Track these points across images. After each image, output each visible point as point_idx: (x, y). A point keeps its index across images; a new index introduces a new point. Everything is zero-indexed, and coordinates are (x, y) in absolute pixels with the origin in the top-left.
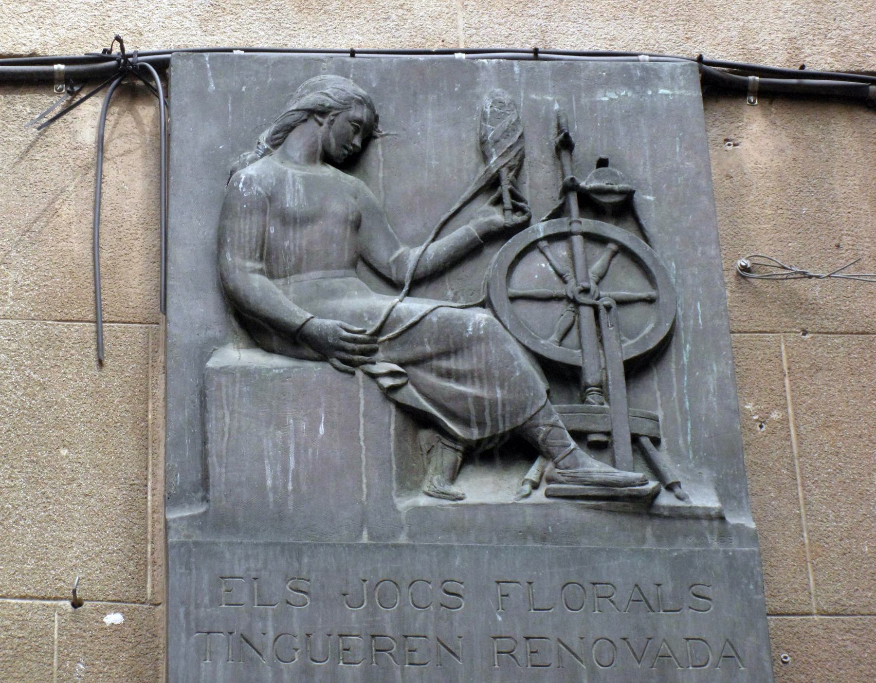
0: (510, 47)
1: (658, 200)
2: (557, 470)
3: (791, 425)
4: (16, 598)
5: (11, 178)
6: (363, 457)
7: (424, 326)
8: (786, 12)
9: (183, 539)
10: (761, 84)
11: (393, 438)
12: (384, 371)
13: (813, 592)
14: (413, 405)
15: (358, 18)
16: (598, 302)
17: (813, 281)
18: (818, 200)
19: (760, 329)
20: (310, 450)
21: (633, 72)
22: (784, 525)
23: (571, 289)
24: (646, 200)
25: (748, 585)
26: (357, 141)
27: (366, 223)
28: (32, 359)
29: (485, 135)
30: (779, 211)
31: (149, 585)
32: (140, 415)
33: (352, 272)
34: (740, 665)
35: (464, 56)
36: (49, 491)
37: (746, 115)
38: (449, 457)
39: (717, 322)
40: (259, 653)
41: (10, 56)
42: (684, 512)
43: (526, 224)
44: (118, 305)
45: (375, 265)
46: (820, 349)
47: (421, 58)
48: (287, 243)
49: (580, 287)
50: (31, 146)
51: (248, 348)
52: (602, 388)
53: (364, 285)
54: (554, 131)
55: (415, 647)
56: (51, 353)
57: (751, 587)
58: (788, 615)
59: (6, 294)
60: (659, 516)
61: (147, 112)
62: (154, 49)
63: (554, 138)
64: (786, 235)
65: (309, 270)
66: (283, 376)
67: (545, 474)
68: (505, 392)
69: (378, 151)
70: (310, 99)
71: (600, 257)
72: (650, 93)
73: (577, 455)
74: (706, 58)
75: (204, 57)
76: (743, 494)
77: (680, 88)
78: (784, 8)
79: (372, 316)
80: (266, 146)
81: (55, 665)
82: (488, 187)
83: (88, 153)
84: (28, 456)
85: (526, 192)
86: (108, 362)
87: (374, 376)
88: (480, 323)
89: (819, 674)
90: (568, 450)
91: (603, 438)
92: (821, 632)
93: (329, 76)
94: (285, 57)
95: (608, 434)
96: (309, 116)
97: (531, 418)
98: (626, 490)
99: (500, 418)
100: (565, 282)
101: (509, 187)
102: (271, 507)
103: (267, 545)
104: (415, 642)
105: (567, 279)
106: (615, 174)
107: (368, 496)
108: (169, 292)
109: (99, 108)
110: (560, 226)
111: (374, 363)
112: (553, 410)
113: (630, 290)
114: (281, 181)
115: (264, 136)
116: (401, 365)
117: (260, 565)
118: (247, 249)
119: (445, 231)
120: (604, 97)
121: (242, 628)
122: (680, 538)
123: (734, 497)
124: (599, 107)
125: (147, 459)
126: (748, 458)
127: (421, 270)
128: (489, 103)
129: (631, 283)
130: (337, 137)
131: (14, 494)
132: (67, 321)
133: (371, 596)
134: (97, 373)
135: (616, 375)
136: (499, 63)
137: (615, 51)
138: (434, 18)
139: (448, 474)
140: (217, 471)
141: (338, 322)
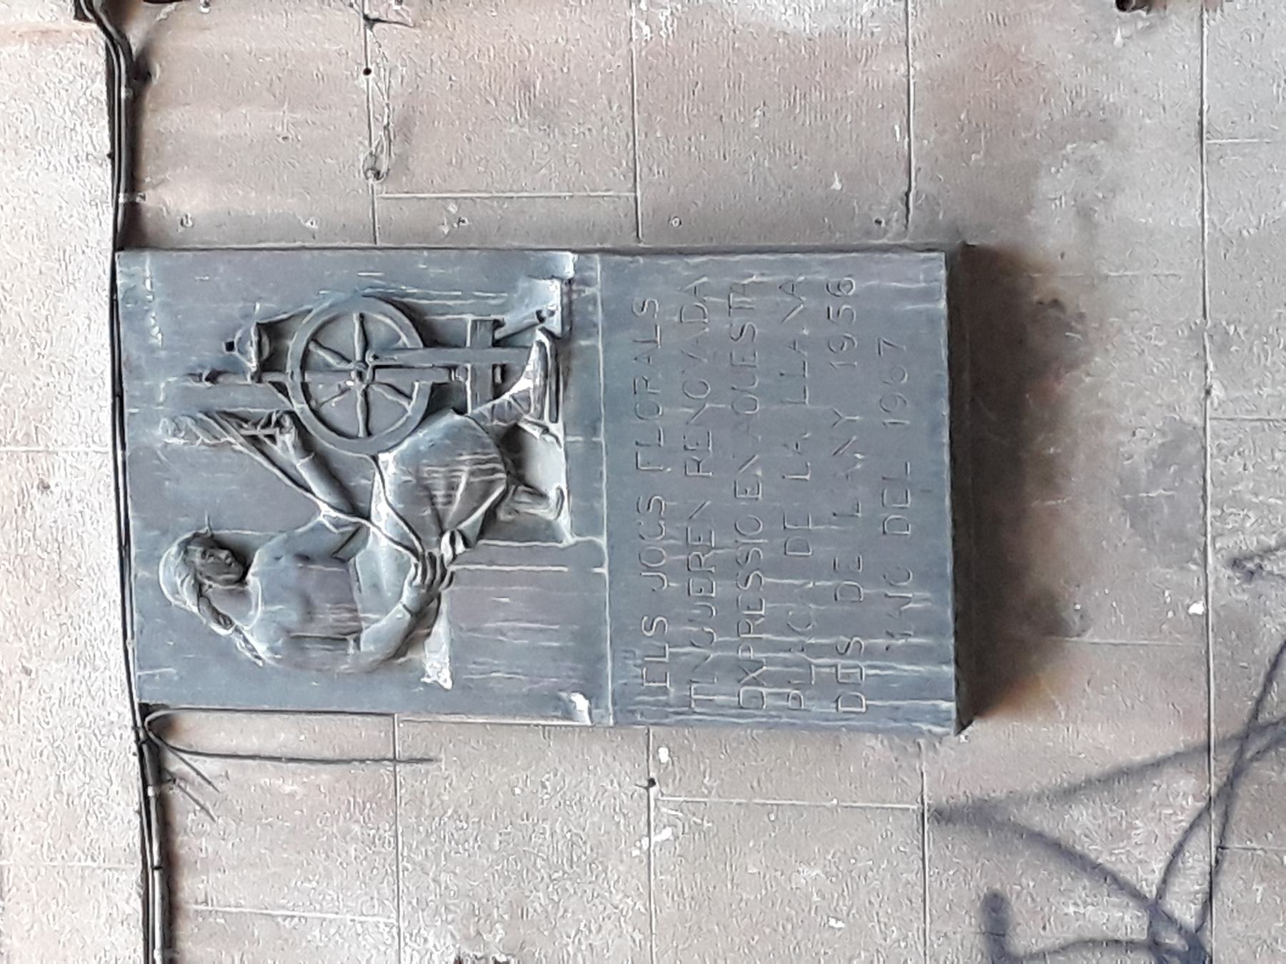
1: (259, 299)
16: (370, 365)
26: (223, 554)
43: (292, 414)
52: (451, 368)
80: (230, 631)
82: (333, 521)
88: (401, 470)
91: (498, 371)
95: (494, 367)
115: (221, 631)
116: (442, 533)
119: (302, 482)
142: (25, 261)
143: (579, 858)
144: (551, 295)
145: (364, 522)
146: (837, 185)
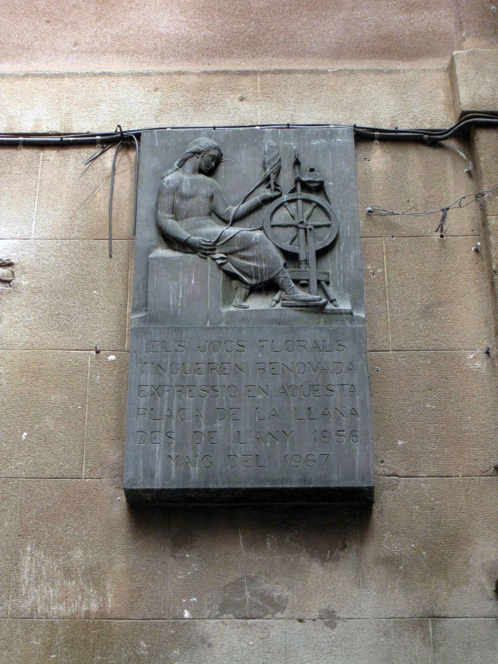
0: (279, 124)
2: (286, 296)
3: (386, 274)
4: (74, 350)
5: (78, 182)
6: (209, 292)
7: (235, 239)
8: (391, 106)
9: (136, 326)
10: (380, 135)
11: (221, 284)
12: (218, 257)
13: (390, 342)
14: (230, 271)
15: (218, 113)
17: (397, 216)
18: (401, 182)
19: (374, 236)
20: (188, 290)
21: (327, 132)
22: (380, 315)
23: (296, 222)
24: (329, 185)
25: (360, 340)
26: (213, 164)
27: (215, 197)
28: (83, 255)
29: (265, 160)
30: (385, 187)
31: (126, 344)
32: (125, 276)
33: (209, 217)
34: (355, 372)
35: (259, 127)
36: (88, 308)
37: (373, 148)
38: (244, 291)
39: (356, 234)
40: (164, 371)
41: (79, 134)
42: (336, 311)
43: (280, 195)
44: (118, 232)
45: (218, 214)
46: (399, 243)
47: (241, 129)
48: (182, 207)
49: (299, 221)
50: (86, 170)
51: (166, 249)
52: (306, 261)
53: (213, 222)
54: (293, 157)
55: (226, 367)
56: (91, 253)
57: (361, 341)
58: (380, 351)
59: (74, 229)
60: (326, 313)
61: (132, 154)
62: (136, 129)
63: (293, 160)
64: (388, 197)
65: (191, 216)
66: (179, 260)
67: (282, 297)
68: (266, 264)
69: (222, 168)
70: (194, 148)
71: (309, 208)
72: (333, 141)
73: (295, 289)
74: (358, 125)
75: (154, 131)
76: (362, 303)
77: (345, 138)
78: (391, 104)
79: (214, 235)
80: (177, 167)
81: (89, 376)
83: (109, 171)
84: (81, 294)
85: (281, 182)
86: (113, 255)
87: (214, 259)
88: (257, 237)
89: (391, 375)
90: (291, 287)
92: (393, 358)
93: (204, 138)
94: (187, 130)
95: (308, 280)
96: (193, 155)
97: (277, 275)
98: (313, 303)
99: (264, 275)
100: (294, 219)
101: (274, 181)
102: (172, 313)
103: (169, 328)
104: (226, 366)
105: (295, 218)
106: (316, 174)
107: (210, 307)
108: (136, 227)
109: (114, 153)
110: (293, 196)
111: (215, 254)
112: (286, 271)
113: (320, 221)
114: (181, 181)
115: (176, 163)
116: (226, 254)
117: (166, 336)
118: (167, 209)
120: (315, 143)
121: (158, 361)
122: (334, 322)
123: (359, 305)
124: (312, 147)
125: (127, 293)
126: (365, 288)
127: (237, 215)
128: (267, 147)
129: (321, 219)
130: (204, 162)
131: (75, 309)
132: (98, 239)
133: (209, 348)
134: (109, 260)
135: (312, 257)
136: (273, 130)
137: (321, 123)
138: (249, 112)
139: (243, 298)
140: (151, 299)
141: (201, 238)
142: (346, 95)
143: (61, 318)
144: (345, 306)
145: (230, 223)
146: (400, 443)
